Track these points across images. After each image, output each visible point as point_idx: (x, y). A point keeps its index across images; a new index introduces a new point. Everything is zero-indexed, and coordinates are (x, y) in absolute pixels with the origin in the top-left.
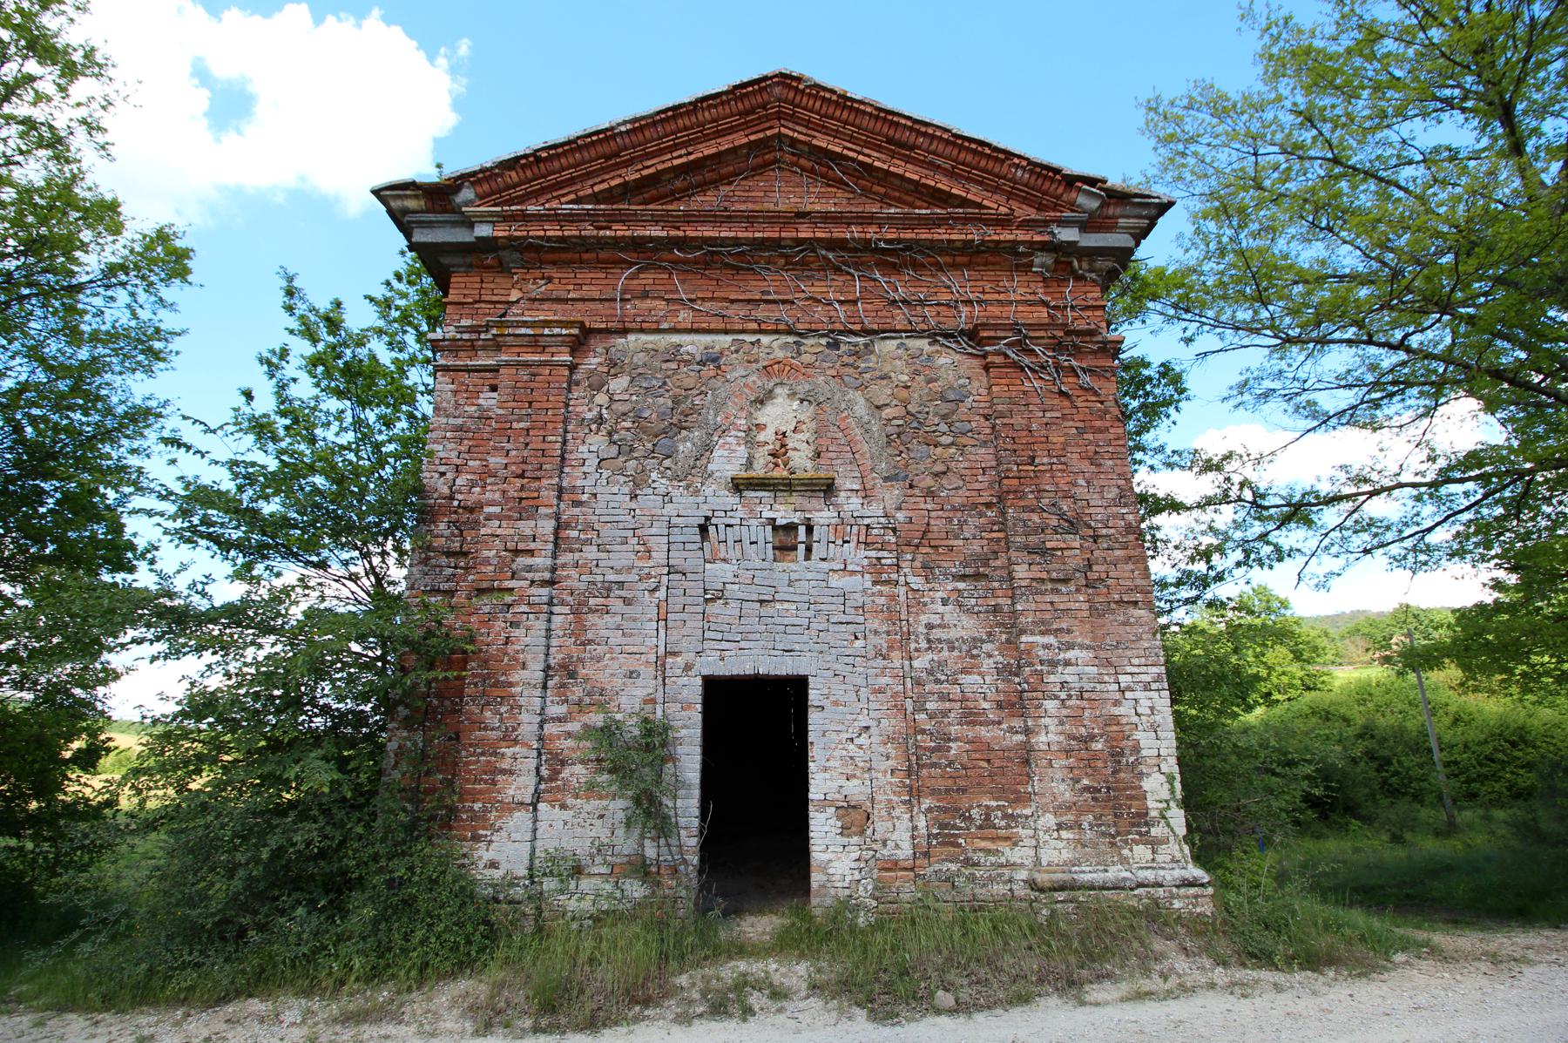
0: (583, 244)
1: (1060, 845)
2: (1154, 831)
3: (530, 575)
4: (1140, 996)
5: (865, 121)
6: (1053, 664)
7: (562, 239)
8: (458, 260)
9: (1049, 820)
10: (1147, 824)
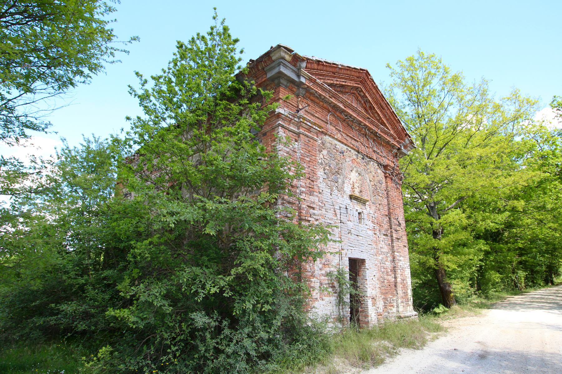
0: (324, 100)
3: (314, 217)
5: (378, 96)
7: (320, 95)
8: (285, 83)
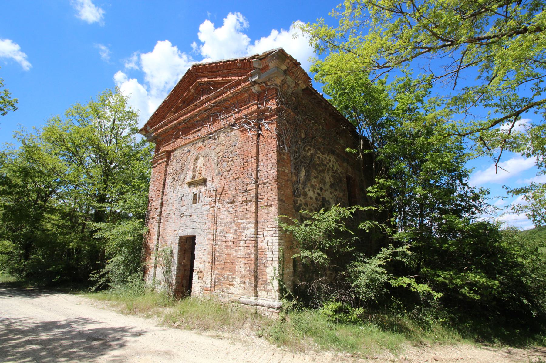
1: (240, 288)
2: (268, 287)
4: (219, 337)
6: (244, 229)
9: (238, 280)
10: (266, 284)
